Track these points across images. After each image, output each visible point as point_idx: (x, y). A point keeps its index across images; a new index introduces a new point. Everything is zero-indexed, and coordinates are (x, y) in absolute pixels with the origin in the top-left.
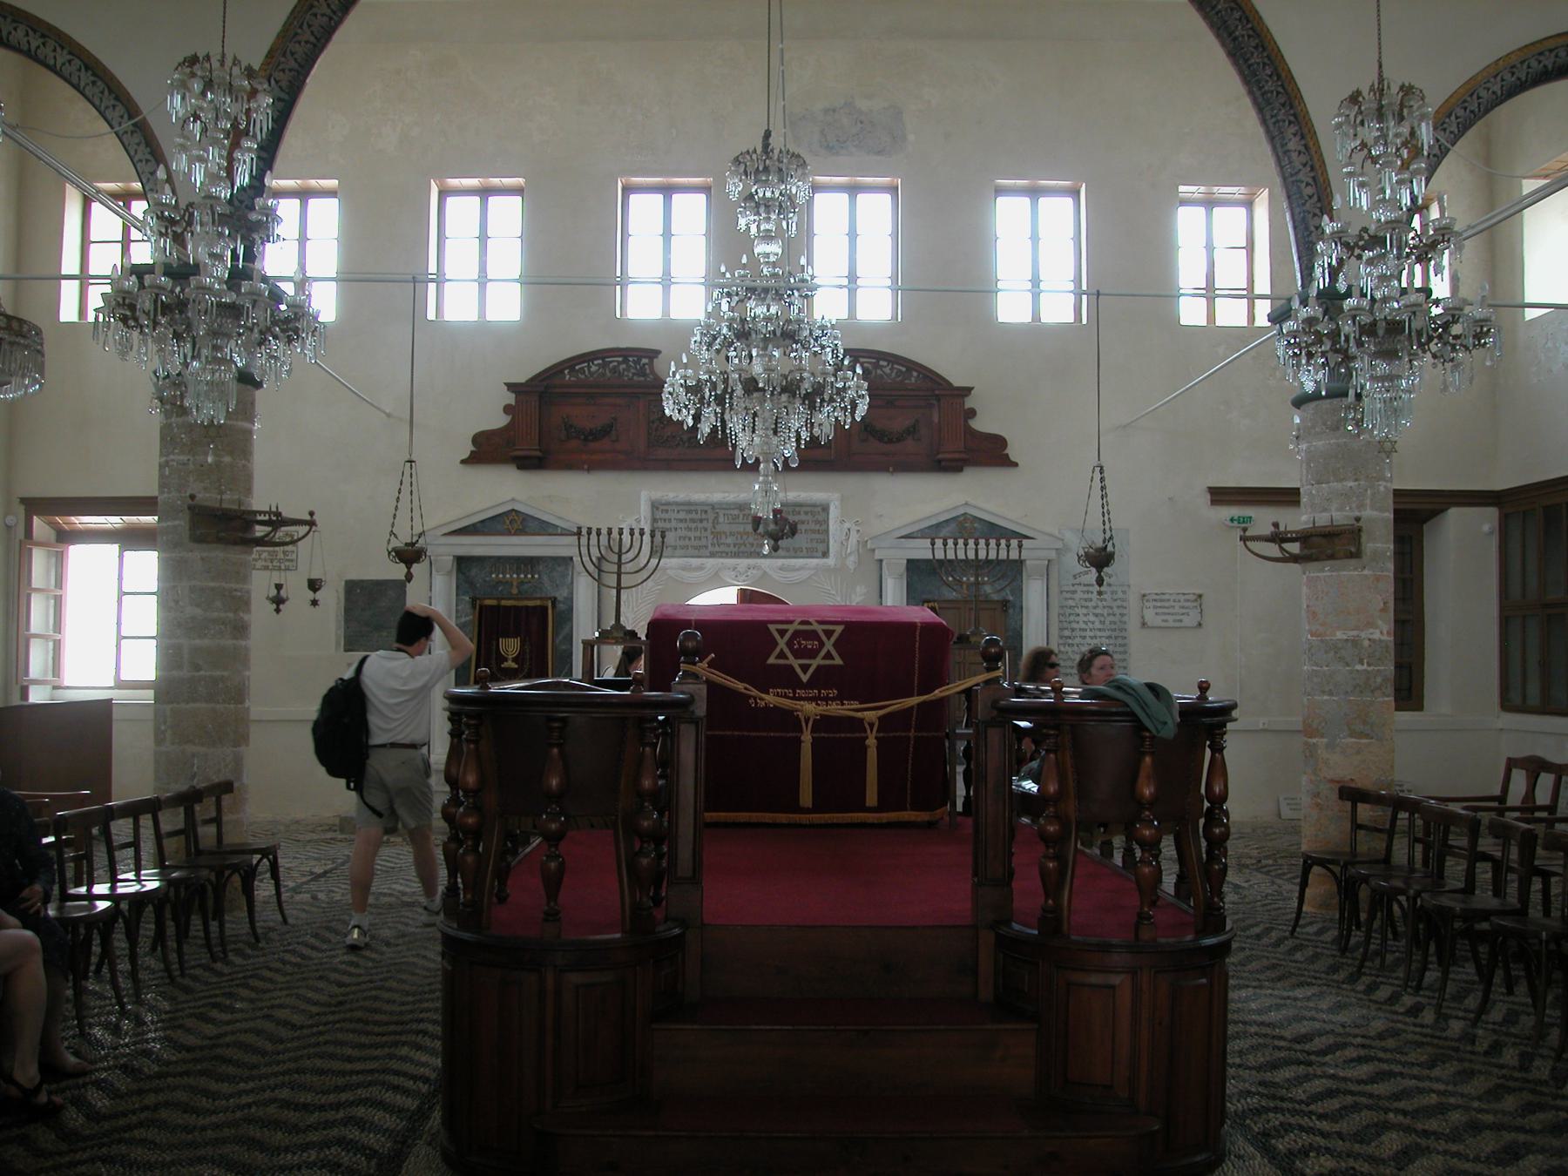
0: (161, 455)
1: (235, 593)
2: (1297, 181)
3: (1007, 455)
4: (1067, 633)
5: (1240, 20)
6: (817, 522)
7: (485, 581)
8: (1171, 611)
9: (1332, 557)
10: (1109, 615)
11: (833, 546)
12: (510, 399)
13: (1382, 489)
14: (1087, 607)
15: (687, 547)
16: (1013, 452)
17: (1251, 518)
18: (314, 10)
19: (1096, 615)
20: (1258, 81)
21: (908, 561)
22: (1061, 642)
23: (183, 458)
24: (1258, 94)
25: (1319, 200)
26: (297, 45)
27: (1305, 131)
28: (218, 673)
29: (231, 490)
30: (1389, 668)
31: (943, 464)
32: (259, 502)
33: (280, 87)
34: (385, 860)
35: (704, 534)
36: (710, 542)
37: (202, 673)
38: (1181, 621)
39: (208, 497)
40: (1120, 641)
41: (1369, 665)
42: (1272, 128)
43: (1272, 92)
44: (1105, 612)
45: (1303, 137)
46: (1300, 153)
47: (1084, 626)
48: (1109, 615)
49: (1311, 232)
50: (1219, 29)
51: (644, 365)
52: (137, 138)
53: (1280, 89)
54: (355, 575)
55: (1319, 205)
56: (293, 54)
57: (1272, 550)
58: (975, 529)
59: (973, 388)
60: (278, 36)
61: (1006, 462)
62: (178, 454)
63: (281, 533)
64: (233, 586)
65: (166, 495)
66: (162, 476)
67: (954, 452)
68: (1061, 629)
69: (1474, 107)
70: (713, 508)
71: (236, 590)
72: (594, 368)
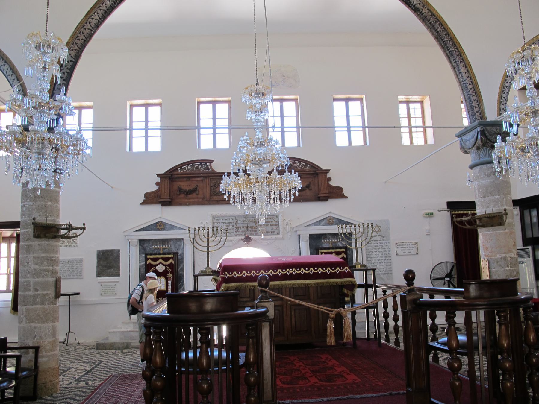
0: (22, 202)
1: (52, 258)
2: (465, 83)
3: (344, 194)
4: (369, 259)
5: (439, 25)
6: (275, 221)
7: (150, 249)
9: (492, 226)
10: (384, 251)
12: (158, 180)
13: (509, 198)
14: (376, 249)
16: (345, 193)
17: (433, 213)
18: (85, 27)
19: (379, 252)
21: (310, 235)
22: (368, 262)
23: (31, 203)
24: (448, 52)
25: (474, 90)
26: (78, 40)
27: (467, 65)
28: (45, 292)
29: (50, 216)
31: (321, 198)
32: (62, 220)
33: (71, 56)
34: (115, 362)
35: (232, 228)
36: (235, 230)
37: (39, 292)
38: (410, 252)
39: (41, 219)
40: (389, 261)
41: (511, 267)
42: (454, 64)
43: (453, 51)
44: (383, 250)
45: (466, 67)
46: (465, 73)
47: (375, 256)
48: (384, 251)
49: (473, 102)
50: (431, 29)
51: (208, 165)
52: (14, 77)
53: (456, 50)
55: (474, 92)
56: (76, 44)
58: (334, 222)
59: (329, 171)
60: (70, 37)
61: (343, 196)
62: (29, 202)
64: (52, 255)
65: (23, 219)
66: (22, 211)
67: (324, 194)
68: (367, 258)
70: (236, 218)
71: (53, 257)
72: (189, 167)
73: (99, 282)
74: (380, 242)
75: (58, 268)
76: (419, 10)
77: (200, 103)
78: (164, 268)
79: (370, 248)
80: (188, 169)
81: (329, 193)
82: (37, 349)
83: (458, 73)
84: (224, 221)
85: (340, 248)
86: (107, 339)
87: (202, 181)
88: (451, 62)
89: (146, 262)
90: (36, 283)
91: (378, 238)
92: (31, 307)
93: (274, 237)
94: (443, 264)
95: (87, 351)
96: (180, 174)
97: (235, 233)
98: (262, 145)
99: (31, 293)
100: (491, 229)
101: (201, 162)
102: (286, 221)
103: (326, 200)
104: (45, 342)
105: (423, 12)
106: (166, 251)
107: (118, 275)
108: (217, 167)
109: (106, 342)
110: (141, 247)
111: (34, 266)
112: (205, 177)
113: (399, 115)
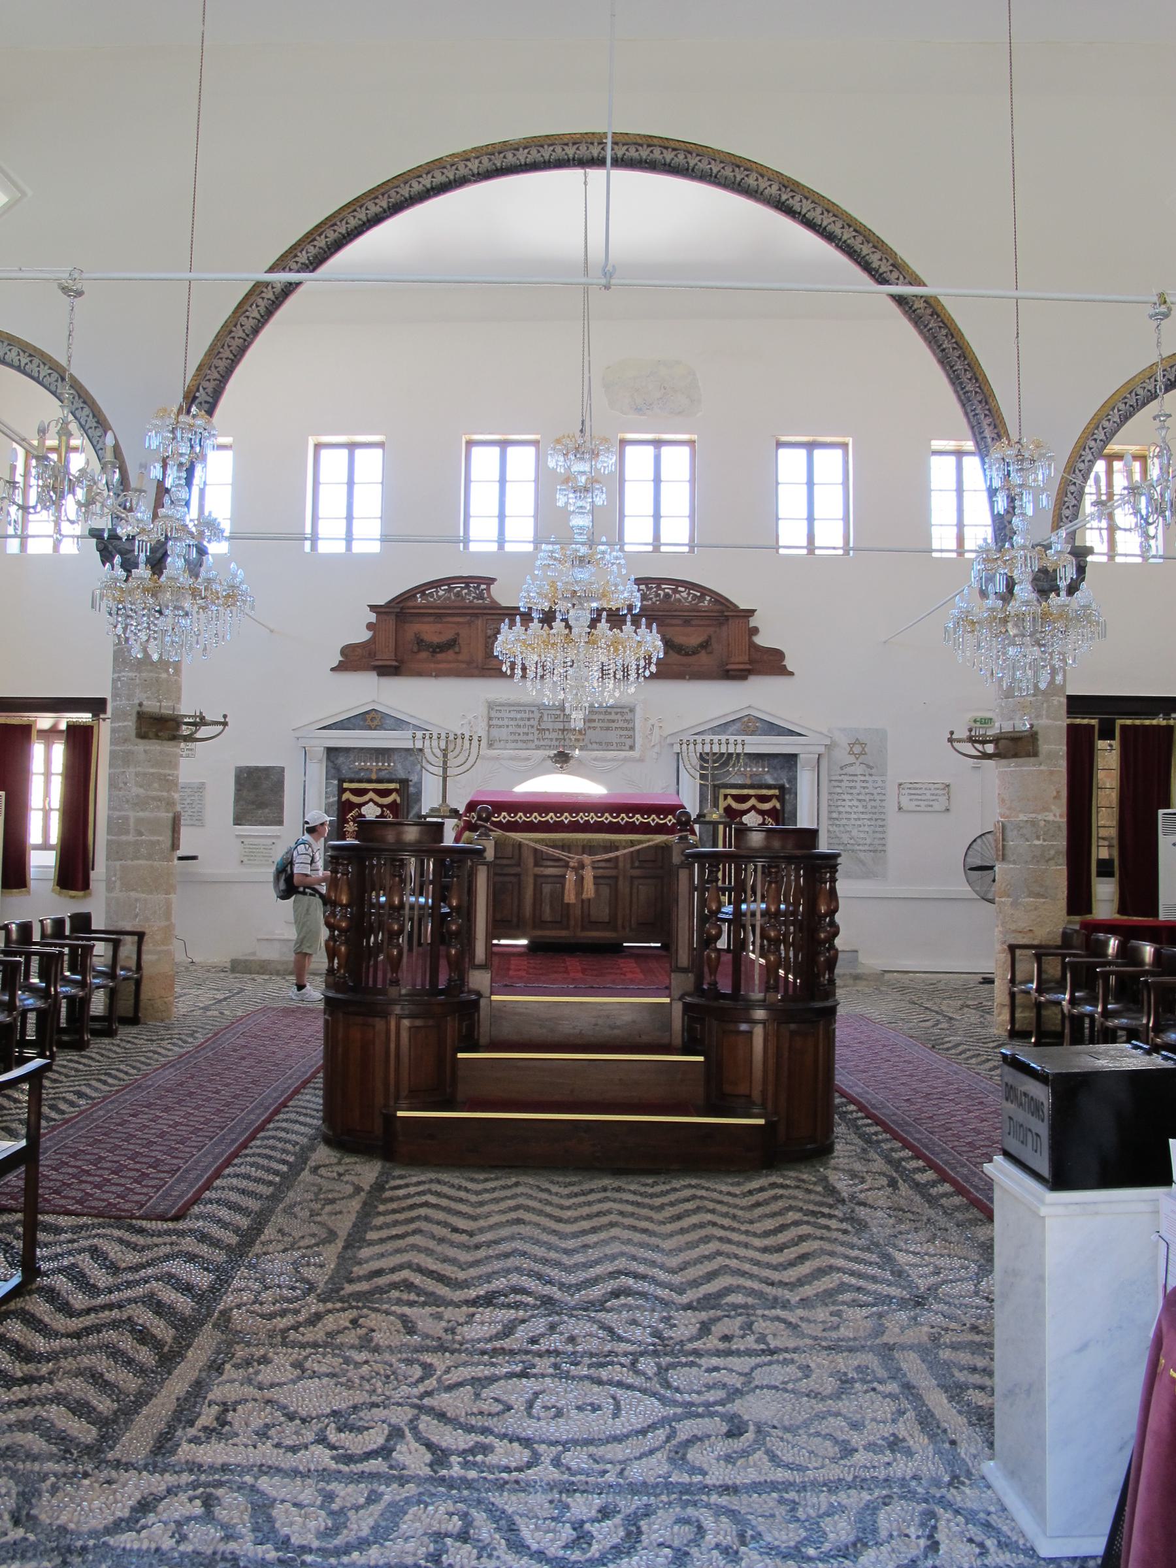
0: (114, 672)
4: (835, 815)
6: (626, 721)
8: (923, 797)
9: (1015, 756)
11: (639, 741)
12: (372, 618)
13: (1055, 702)
15: (516, 741)
16: (789, 663)
19: (860, 800)
20: (961, 383)
27: (998, 422)
28: (155, 838)
30: (1062, 843)
32: (186, 708)
35: (531, 730)
44: (868, 798)
45: (995, 427)
47: (849, 810)
54: (1065, 911)
57: (968, 748)
61: (784, 671)
63: (203, 732)
64: (168, 772)
68: (830, 812)
69: (1133, 402)
72: (441, 593)
73: (238, 836)
74: (863, 778)
75: (176, 796)
76: (907, 303)
77: (470, 444)
78: (378, 811)
79: (838, 790)
80: (439, 597)
81: (751, 662)
82: (141, 936)
83: (979, 437)
84: (513, 715)
85: (769, 787)
86: (254, 954)
87: (469, 623)
88: (966, 414)
89: (340, 797)
90: (139, 821)
91: (858, 769)
92: (129, 862)
93: (623, 754)
94: (989, 836)
95: (211, 975)
96: (420, 608)
97: (536, 742)
98: (582, 561)
99: (131, 838)
100: (1013, 762)
101: (467, 581)
102: (651, 722)
103: (744, 678)
104: (153, 929)
105: (915, 307)
106: (383, 774)
107: (280, 822)
108: (502, 595)
109: (252, 958)
110: (330, 764)
111: (136, 790)
112: (476, 615)
113: (929, 485)
